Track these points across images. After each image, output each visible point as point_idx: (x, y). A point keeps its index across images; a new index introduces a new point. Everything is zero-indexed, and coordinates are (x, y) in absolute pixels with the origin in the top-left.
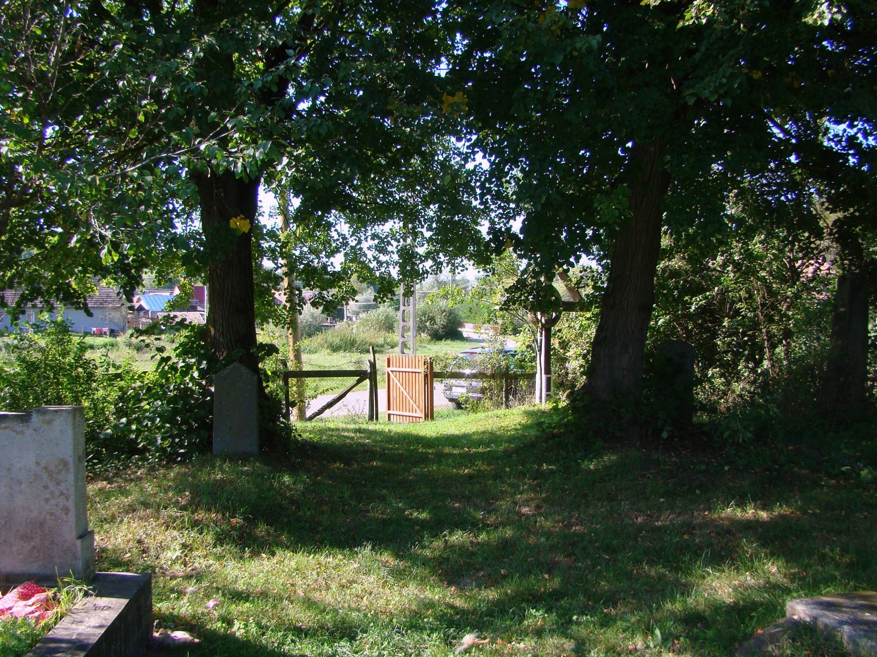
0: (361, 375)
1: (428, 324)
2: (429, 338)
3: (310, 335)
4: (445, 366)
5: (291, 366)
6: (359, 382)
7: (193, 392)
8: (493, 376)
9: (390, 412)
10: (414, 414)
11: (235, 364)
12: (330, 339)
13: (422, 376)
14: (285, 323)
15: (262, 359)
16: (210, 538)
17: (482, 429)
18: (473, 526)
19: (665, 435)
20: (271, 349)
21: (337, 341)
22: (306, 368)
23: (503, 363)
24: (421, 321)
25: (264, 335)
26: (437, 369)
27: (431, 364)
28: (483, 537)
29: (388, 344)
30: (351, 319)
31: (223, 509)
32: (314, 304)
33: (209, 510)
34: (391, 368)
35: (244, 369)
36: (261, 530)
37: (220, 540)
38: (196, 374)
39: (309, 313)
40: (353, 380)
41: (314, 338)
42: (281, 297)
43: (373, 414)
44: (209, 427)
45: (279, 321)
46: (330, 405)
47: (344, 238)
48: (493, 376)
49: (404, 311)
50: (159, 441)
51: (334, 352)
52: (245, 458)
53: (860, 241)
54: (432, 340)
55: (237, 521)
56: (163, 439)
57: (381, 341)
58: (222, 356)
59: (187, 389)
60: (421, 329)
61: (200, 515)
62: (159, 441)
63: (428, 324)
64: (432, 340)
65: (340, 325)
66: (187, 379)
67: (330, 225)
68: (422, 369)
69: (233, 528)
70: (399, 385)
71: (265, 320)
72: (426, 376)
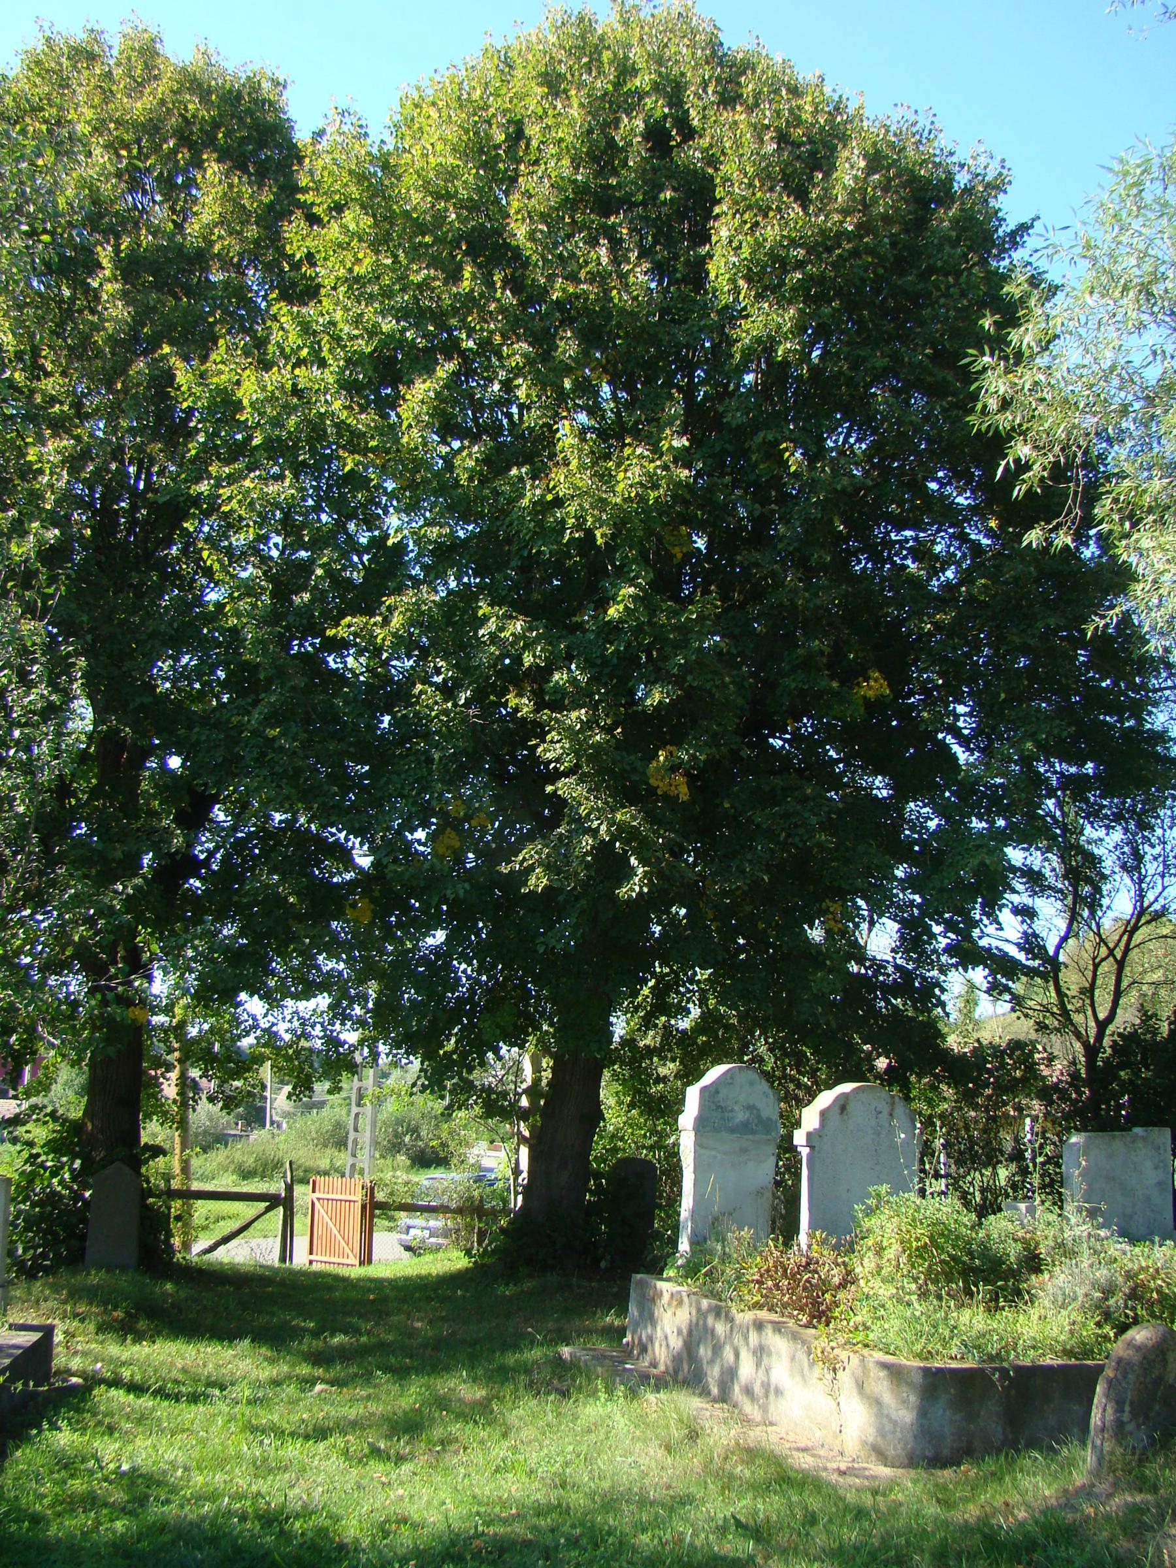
0: (273, 1201)
1: (407, 1139)
2: (408, 1162)
3: (205, 1150)
4: (392, 1194)
5: (175, 1184)
6: (268, 1210)
7: (62, 1197)
8: (460, 1211)
9: (312, 1257)
10: (345, 1261)
11: (117, 1164)
12: (238, 1156)
13: (359, 1205)
14: (173, 1122)
15: (146, 1162)
16: (92, 1327)
17: (424, 1272)
18: (357, 1332)
19: (603, 1264)
20: (157, 1151)
21: (250, 1162)
22: (196, 1186)
23: (476, 1193)
24: (397, 1135)
25: (152, 1131)
26: (380, 1196)
27: (372, 1189)
28: (364, 1339)
29: (336, 1170)
30: (279, 1126)
31: (105, 1303)
32: (211, 1099)
33: (91, 1304)
34: (317, 1195)
35: (127, 1170)
36: (142, 1324)
37: (100, 1329)
38: (67, 1176)
39: (205, 1112)
40: (263, 1205)
41: (212, 1154)
42: (170, 1090)
43: (286, 1251)
44: (83, 1237)
45: (165, 1116)
46: (225, 1240)
47: (254, 1018)
48: (460, 1211)
49: (357, 1115)
50: (20, 1251)
51: (244, 1178)
52: (124, 1268)
53: (448, 1084)
54: (412, 1166)
55: (119, 1314)
56: (25, 1250)
57: (324, 1164)
58: (98, 1155)
59: (54, 1193)
60: (395, 1147)
61: (81, 1309)
62: (20, 1251)
63: (407, 1139)
64: (412, 1166)
65: (257, 1135)
66: (55, 1180)
67: (240, 1004)
68: (358, 1196)
69: (116, 1320)
70: (327, 1219)
71: (148, 1116)
72: (364, 1207)
